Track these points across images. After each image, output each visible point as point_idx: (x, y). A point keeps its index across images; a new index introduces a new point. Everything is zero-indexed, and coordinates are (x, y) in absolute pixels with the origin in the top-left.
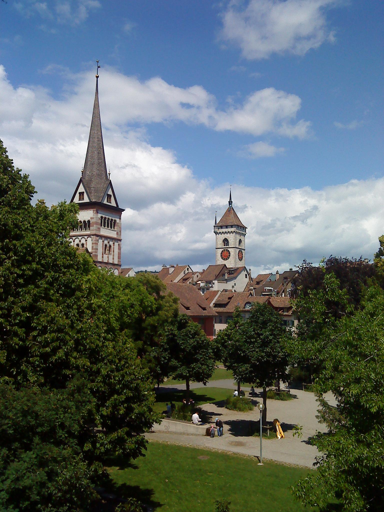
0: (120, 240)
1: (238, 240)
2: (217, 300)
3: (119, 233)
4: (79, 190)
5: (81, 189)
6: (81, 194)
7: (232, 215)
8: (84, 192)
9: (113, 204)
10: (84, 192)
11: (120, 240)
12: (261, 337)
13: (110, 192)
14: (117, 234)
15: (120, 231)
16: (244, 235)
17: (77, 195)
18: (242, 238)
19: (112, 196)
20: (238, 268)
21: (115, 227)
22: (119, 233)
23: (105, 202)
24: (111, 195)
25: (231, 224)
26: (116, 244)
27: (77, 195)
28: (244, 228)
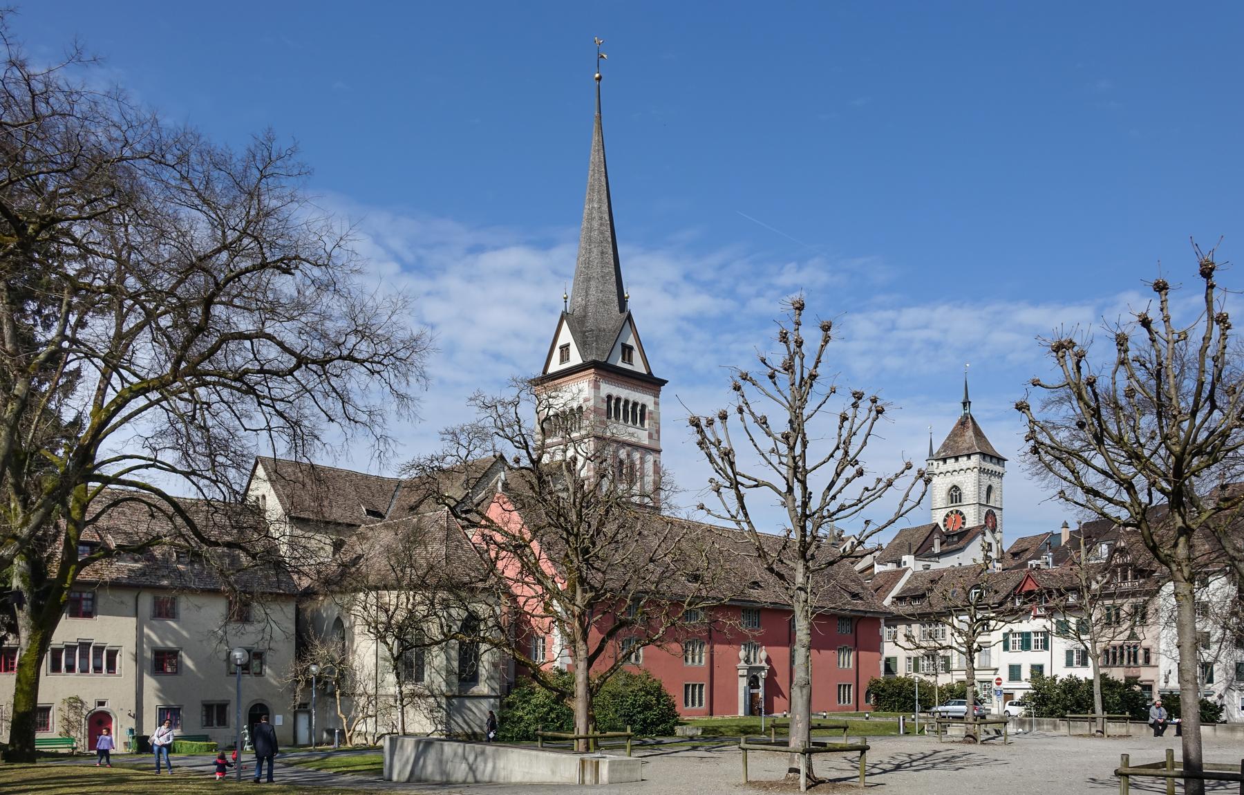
0: (659, 452)
1: (984, 489)
2: (904, 591)
3: (655, 436)
4: (560, 342)
5: (566, 336)
6: (565, 348)
7: (970, 433)
8: (568, 345)
9: (638, 366)
10: (568, 345)
11: (659, 452)
12: (151, 306)
13: (631, 341)
14: (650, 436)
15: (658, 432)
16: (1000, 476)
17: (557, 352)
18: (995, 481)
19: (636, 347)
20: (968, 530)
21: (646, 422)
22: (655, 434)
23: (620, 364)
24: (631, 348)
25: (966, 452)
26: (650, 458)
27: (557, 352)
28: (1000, 460)
